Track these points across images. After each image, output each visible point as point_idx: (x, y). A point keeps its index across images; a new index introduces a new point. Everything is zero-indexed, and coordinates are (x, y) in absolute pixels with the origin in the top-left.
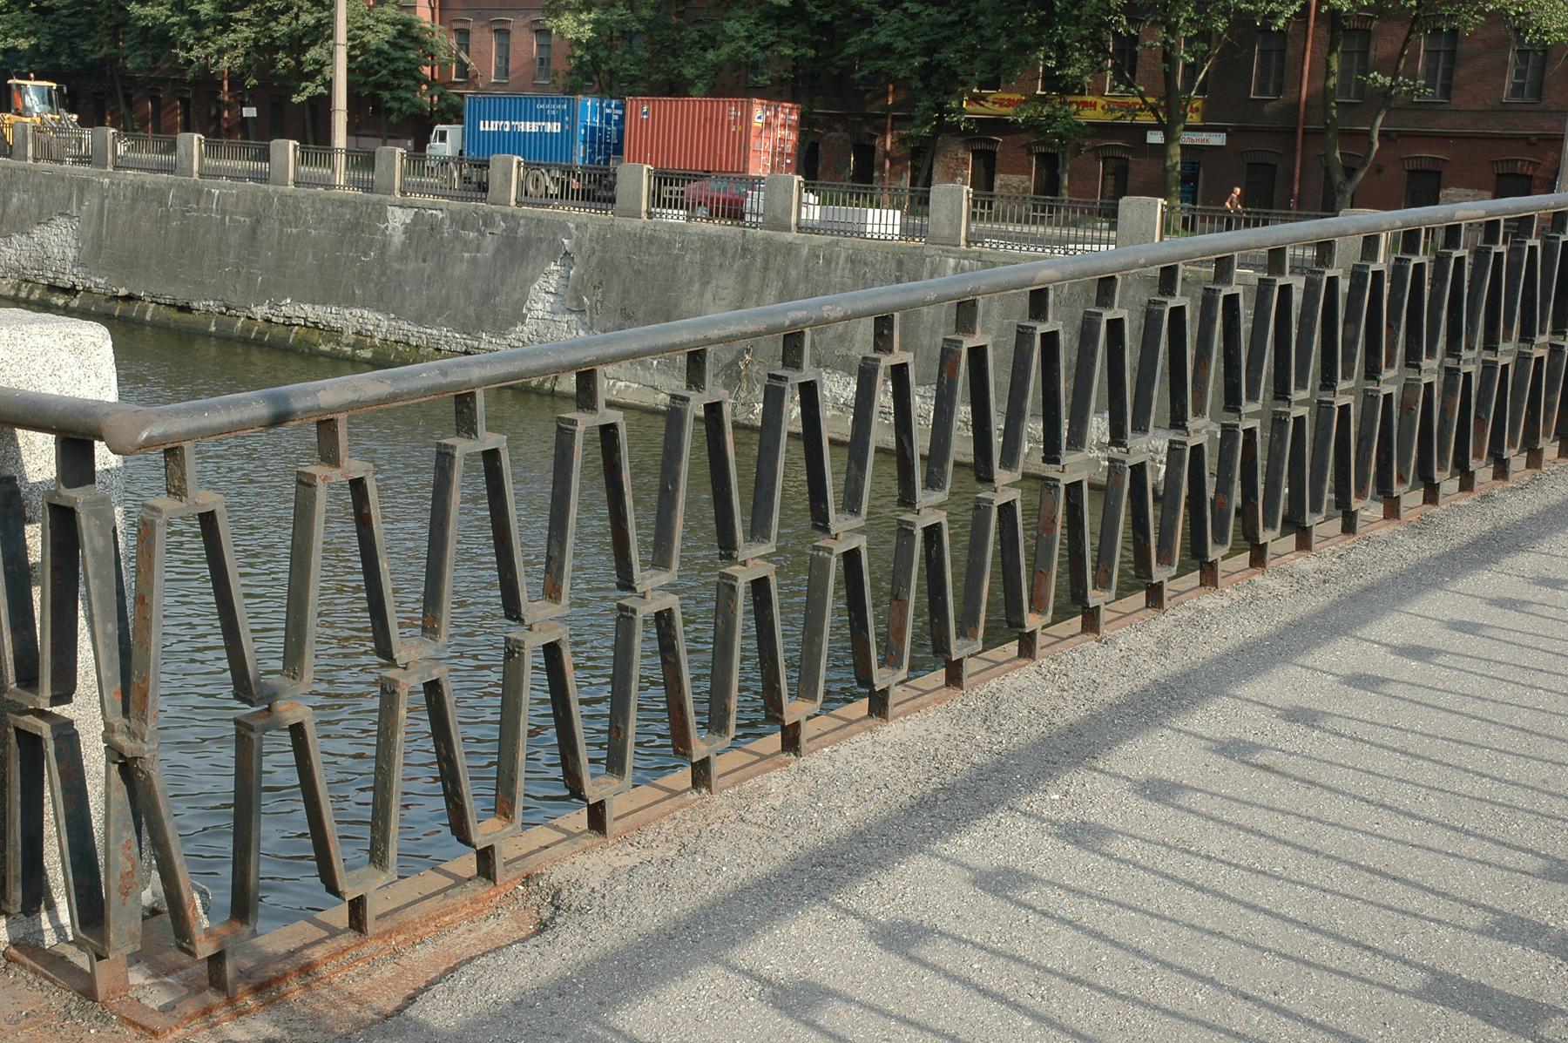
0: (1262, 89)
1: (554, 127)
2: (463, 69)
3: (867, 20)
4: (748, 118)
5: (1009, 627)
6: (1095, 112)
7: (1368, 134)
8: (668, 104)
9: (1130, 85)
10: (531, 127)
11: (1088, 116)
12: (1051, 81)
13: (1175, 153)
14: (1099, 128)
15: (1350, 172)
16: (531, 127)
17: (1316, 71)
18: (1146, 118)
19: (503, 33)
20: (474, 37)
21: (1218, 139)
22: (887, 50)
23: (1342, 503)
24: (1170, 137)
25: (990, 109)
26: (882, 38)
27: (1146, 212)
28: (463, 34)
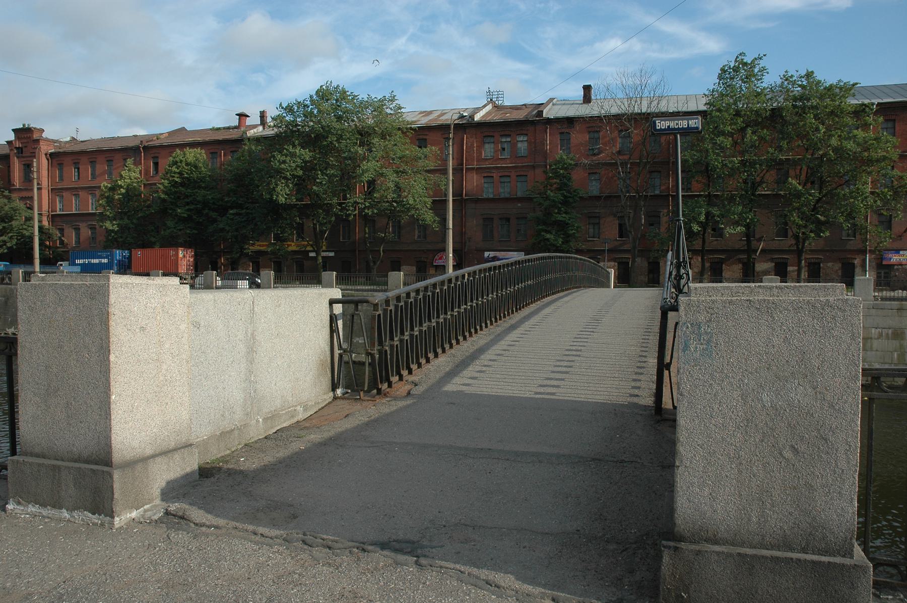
0: (344, 238)
1: (105, 261)
2: (62, 242)
3: (215, 221)
4: (177, 254)
5: (781, 272)
6: (293, 247)
7: (379, 251)
8: (148, 251)
9: (303, 238)
10: (96, 261)
11: (290, 249)
12: (277, 238)
13: (320, 258)
14: (294, 252)
15: (375, 263)
16: (96, 261)
17: (359, 232)
18: (309, 248)
19: (77, 229)
20: (66, 231)
21: (332, 254)
22: (222, 230)
23: (418, 359)
24: (318, 253)
25: (256, 248)
26: (221, 226)
27: (397, 278)
28: (62, 230)
